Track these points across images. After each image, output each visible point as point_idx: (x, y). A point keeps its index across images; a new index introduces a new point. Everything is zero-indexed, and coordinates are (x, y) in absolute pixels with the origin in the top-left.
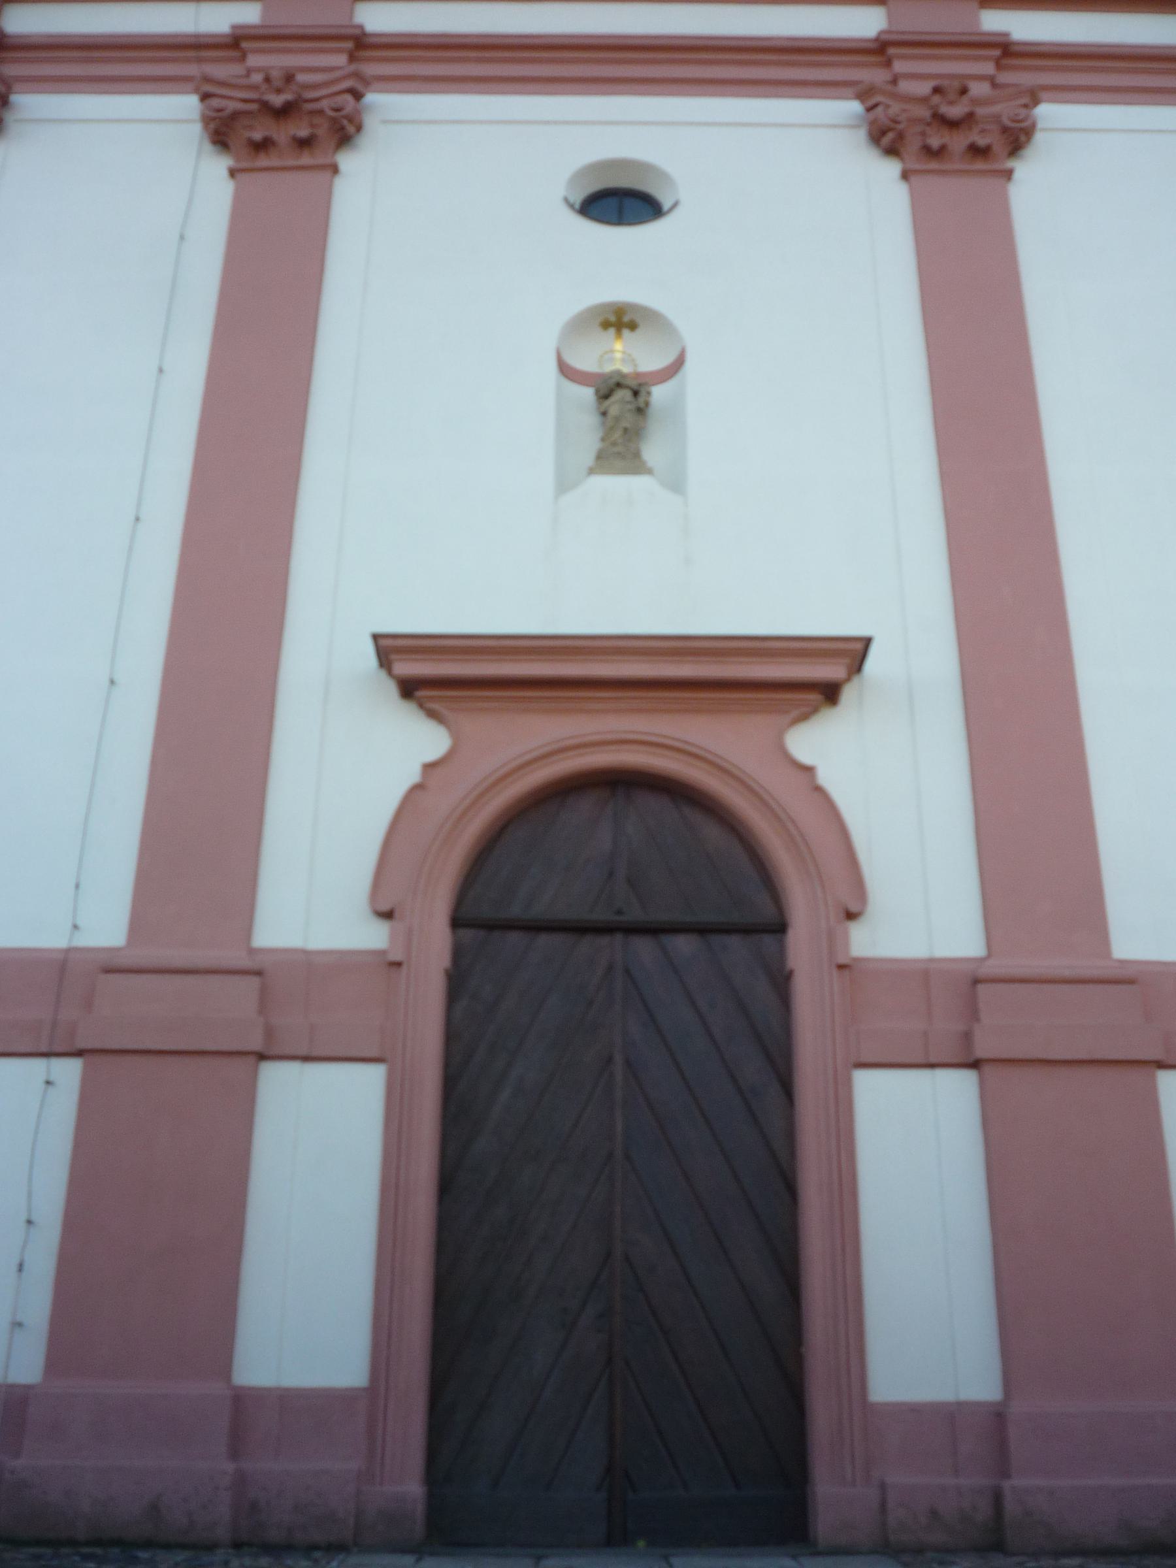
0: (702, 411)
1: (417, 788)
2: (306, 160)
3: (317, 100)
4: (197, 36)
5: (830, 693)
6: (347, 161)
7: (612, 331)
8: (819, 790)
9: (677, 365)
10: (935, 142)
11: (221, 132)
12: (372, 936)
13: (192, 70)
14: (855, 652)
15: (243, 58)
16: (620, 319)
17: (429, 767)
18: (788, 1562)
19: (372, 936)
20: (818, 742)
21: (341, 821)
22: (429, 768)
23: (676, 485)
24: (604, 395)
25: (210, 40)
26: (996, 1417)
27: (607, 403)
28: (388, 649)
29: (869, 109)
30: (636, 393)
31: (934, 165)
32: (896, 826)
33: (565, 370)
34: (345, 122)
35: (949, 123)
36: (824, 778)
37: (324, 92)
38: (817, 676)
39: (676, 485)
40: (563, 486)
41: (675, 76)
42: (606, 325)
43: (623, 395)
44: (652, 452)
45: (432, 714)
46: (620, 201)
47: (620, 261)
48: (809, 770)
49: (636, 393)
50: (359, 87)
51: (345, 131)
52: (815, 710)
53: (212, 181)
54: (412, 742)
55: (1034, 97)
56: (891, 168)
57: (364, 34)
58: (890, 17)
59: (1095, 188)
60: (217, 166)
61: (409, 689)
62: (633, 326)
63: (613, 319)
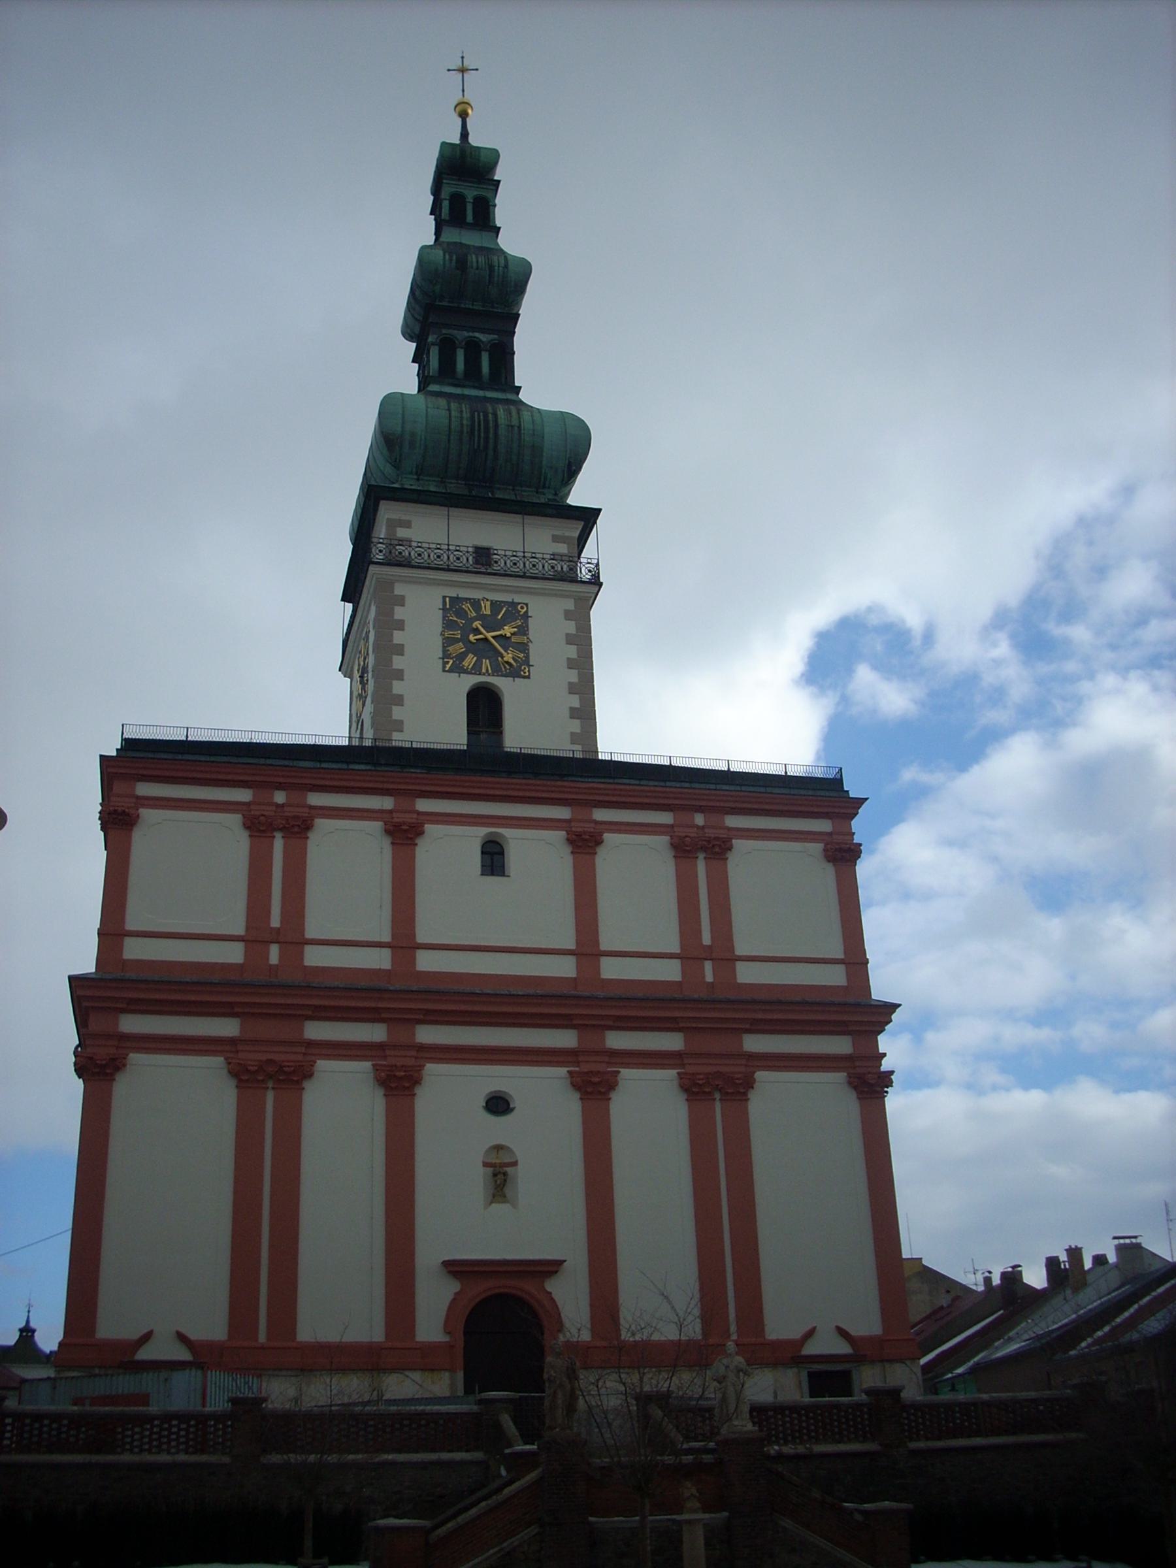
1: (454, 1299)
5: (556, 1272)
8: (552, 1299)
10: (589, 1090)
12: (446, 1339)
14: (560, 1263)
16: (498, 1148)
18: (497, 209)
19: (446, 1339)
20: (551, 1286)
21: (434, 1308)
23: (515, 1206)
24: (495, 1175)
26: (242, 965)
28: (447, 1264)
32: (571, 1299)
33: (485, 1165)
36: (554, 1296)
38: (551, 1268)
39: (515, 1206)
40: (486, 1208)
43: (501, 1176)
44: (508, 1191)
46: (498, 1105)
47: (499, 1129)
54: (452, 1287)
61: (450, 1272)
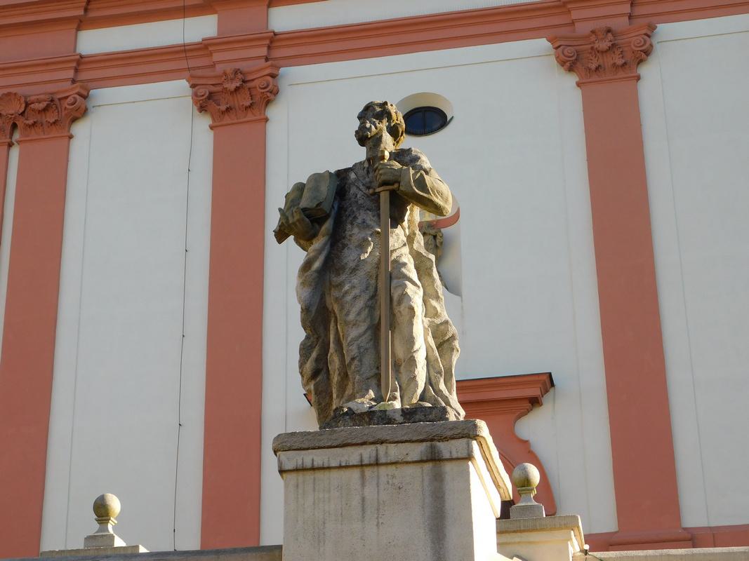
2: (250, 117)
3: (253, 80)
4: (184, 45)
5: (535, 402)
11: (205, 103)
13: (183, 64)
14: (547, 382)
15: (211, 54)
25: (451, 501)
29: (193, 86)
30: (435, 237)
31: (595, 78)
34: (269, 94)
35: (605, 59)
37: (258, 75)
48: (526, 442)
49: (435, 237)
50: (274, 72)
51: (269, 95)
52: (528, 411)
53: (201, 129)
56: (571, 80)
57: (275, 34)
59: (692, 65)
60: (205, 122)
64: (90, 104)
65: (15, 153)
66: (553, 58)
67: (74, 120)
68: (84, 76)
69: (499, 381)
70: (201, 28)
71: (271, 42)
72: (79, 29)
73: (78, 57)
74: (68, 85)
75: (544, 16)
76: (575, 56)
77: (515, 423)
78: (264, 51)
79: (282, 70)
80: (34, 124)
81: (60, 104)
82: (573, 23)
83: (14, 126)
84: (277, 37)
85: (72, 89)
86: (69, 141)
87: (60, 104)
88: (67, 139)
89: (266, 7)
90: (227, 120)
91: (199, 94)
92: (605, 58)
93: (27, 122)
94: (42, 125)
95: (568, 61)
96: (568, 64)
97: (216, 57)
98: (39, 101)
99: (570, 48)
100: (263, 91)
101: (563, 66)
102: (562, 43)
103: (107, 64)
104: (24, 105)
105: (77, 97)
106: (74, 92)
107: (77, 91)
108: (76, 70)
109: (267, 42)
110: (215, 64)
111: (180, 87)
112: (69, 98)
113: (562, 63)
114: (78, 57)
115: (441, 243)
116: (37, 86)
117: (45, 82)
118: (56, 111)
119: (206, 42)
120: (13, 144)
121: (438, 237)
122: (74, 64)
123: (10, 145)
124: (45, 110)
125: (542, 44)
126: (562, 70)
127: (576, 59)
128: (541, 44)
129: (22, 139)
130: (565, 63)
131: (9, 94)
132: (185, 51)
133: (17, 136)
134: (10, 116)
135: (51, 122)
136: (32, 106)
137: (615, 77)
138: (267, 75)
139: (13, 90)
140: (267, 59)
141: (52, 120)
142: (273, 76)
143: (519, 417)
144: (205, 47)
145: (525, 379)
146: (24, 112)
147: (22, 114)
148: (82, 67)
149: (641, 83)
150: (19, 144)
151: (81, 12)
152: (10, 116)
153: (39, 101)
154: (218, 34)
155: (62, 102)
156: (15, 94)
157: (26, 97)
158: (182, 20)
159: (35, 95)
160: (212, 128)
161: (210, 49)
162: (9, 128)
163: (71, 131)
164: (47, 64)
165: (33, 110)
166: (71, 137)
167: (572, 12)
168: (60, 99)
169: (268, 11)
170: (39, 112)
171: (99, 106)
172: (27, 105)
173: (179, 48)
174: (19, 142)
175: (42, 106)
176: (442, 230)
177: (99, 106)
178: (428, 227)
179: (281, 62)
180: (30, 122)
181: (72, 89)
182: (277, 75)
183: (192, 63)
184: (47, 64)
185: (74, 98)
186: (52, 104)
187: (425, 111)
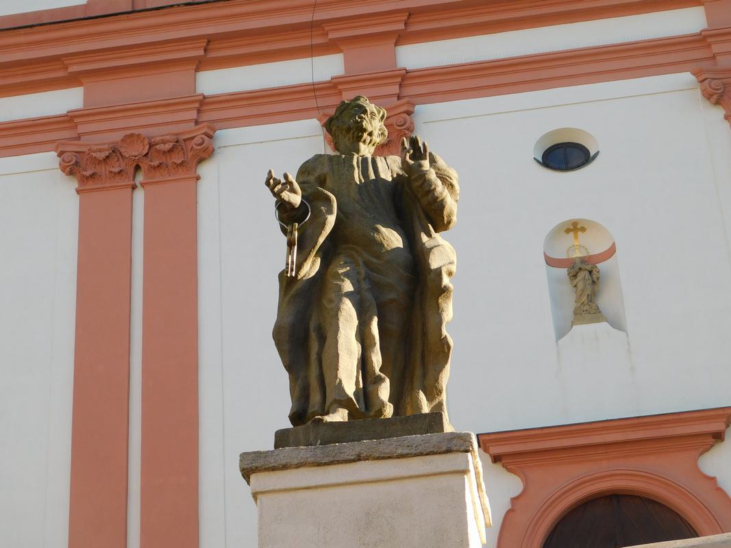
0: (626, 281)
6: (207, 171)
7: (572, 233)
9: (611, 252)
11: (72, 168)
13: (312, 103)
15: (76, 127)
16: (575, 228)
17: (514, 500)
22: (514, 500)
23: (617, 325)
27: (576, 281)
29: (59, 155)
30: (590, 272)
33: (550, 262)
34: (406, 132)
40: (561, 333)
41: (158, 128)
42: (568, 231)
43: (581, 275)
44: (605, 301)
45: (510, 470)
46: (564, 155)
49: (590, 272)
52: (712, 446)
54: (512, 485)
55: (413, 105)
57: (205, 97)
58: (709, 16)
61: (496, 459)
62: (583, 229)
63: (572, 227)
64: (216, 144)
65: (139, 196)
66: (699, 92)
67: (201, 161)
68: (206, 117)
69: (682, 416)
70: (328, 67)
71: (403, 80)
72: (197, 70)
73: (202, 97)
74: (191, 126)
75: (684, 50)
76: (722, 89)
77: (699, 457)
78: (395, 89)
79: (417, 107)
80: (160, 165)
81: (186, 145)
82: (714, 57)
83: (138, 168)
84: (207, 100)
85: (196, 131)
86: (132, 192)
87: (186, 145)
88: (195, 179)
89: (393, 45)
90: (91, 185)
91: (66, 160)
92: (168, 158)
93: (152, 164)
94: (167, 167)
95: (716, 94)
96: (715, 97)
97: (81, 129)
98: (164, 142)
99: (716, 81)
100: (399, 128)
101: (709, 99)
102: (707, 76)
103: (91, 118)
104: (147, 147)
105: (204, 136)
106: (202, 132)
107: (204, 131)
108: (199, 111)
109: (399, 80)
110: (80, 137)
111: (48, 159)
112: (195, 139)
113: (708, 96)
114: (202, 97)
115: (598, 278)
116: (161, 127)
117: (167, 124)
118: (182, 152)
119: (334, 81)
120: (137, 187)
121: (594, 272)
122: (197, 105)
123: (134, 187)
124: (170, 151)
125: (686, 77)
126: (707, 103)
127: (722, 93)
128: (686, 78)
129: (147, 181)
130: (711, 96)
131: (132, 135)
132: (314, 90)
133: (140, 178)
134: (133, 158)
135: (179, 163)
136: (157, 147)
137: (188, 176)
138: (404, 112)
139: (136, 132)
140: (399, 98)
141: (179, 162)
142: (409, 113)
143: (702, 454)
144: (70, 119)
145: (711, 413)
146: (147, 154)
147: (146, 155)
148: (405, 83)
149: (200, 182)
150: (143, 187)
151: (201, 52)
152: (133, 158)
153: (164, 142)
154: (84, 106)
155: (187, 142)
156: (139, 135)
157: (150, 138)
158: (309, 59)
159: (160, 136)
160: (78, 192)
161: (76, 120)
162: (131, 170)
163: (197, 173)
164: (168, 105)
165: (158, 151)
166: (198, 178)
167: (712, 46)
168: (184, 140)
169: (195, 76)
170: (164, 152)
171: (225, 147)
172: (151, 146)
173: (697, 37)
174: (142, 185)
175: (168, 146)
176: (599, 265)
177: (225, 147)
178: (581, 263)
179: (416, 100)
180: (156, 163)
181: (196, 131)
182: (413, 112)
183: (321, 102)
184: (168, 105)
185: (202, 139)
186: (177, 145)
187: (567, 147)
